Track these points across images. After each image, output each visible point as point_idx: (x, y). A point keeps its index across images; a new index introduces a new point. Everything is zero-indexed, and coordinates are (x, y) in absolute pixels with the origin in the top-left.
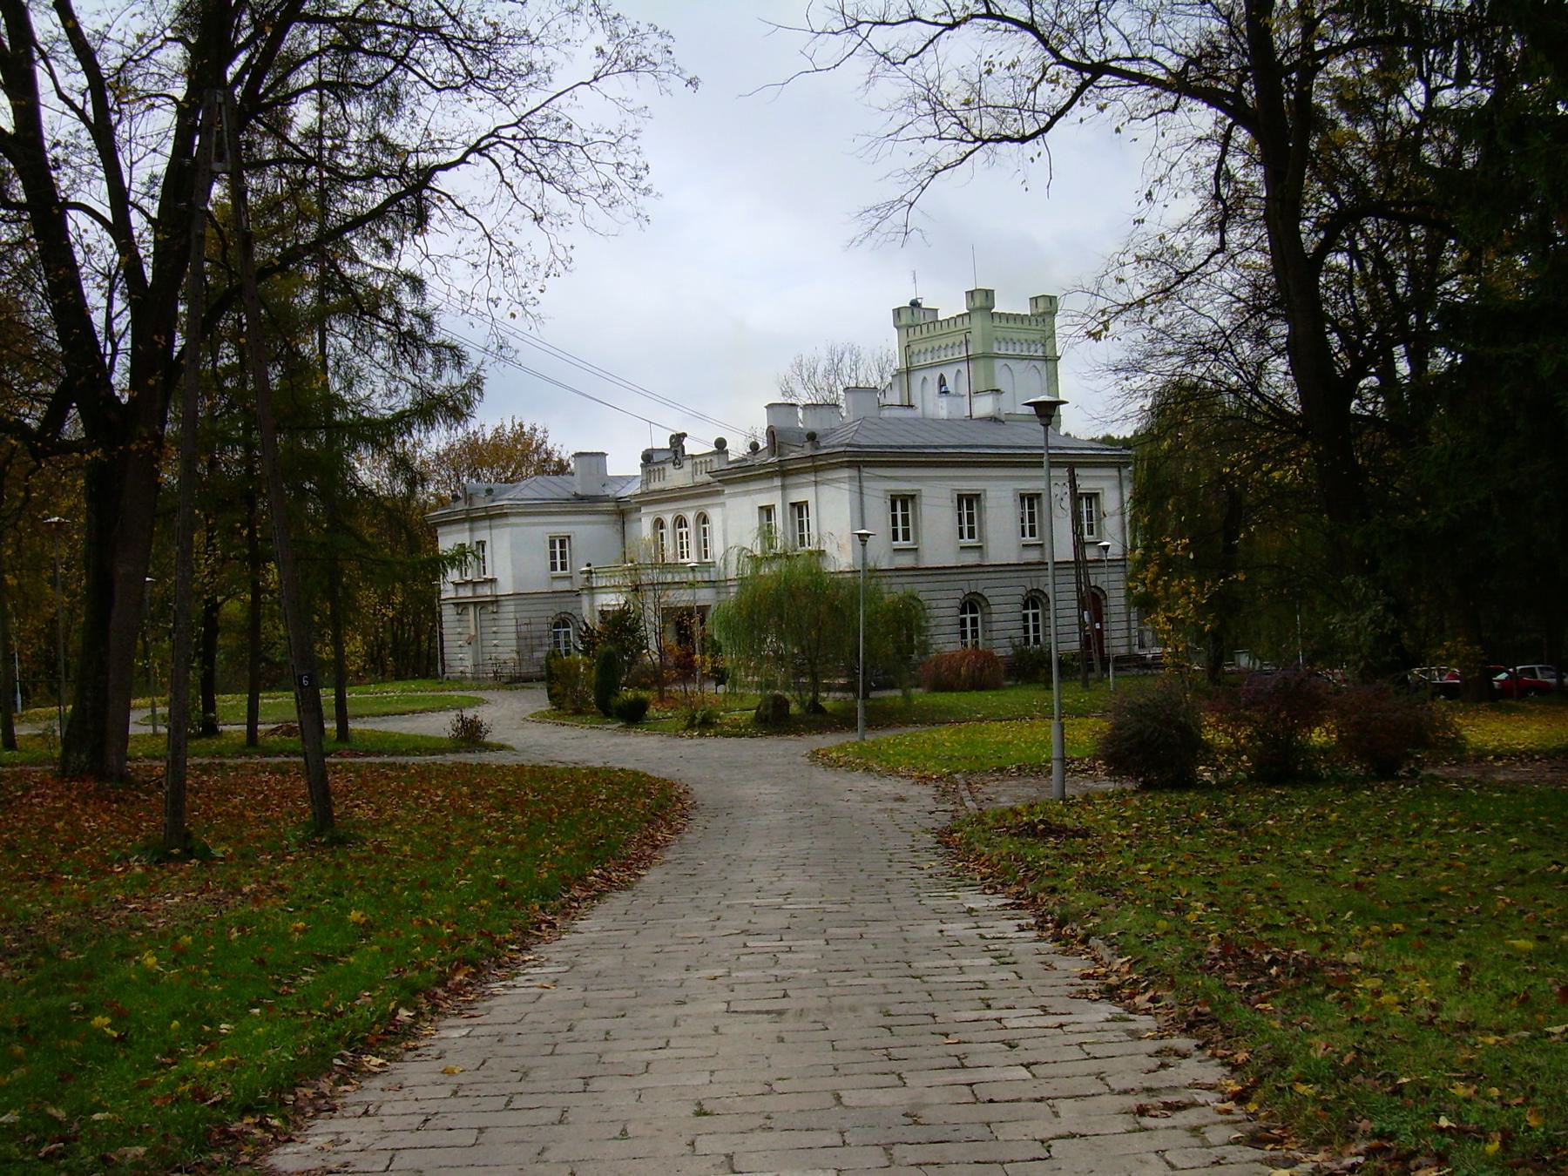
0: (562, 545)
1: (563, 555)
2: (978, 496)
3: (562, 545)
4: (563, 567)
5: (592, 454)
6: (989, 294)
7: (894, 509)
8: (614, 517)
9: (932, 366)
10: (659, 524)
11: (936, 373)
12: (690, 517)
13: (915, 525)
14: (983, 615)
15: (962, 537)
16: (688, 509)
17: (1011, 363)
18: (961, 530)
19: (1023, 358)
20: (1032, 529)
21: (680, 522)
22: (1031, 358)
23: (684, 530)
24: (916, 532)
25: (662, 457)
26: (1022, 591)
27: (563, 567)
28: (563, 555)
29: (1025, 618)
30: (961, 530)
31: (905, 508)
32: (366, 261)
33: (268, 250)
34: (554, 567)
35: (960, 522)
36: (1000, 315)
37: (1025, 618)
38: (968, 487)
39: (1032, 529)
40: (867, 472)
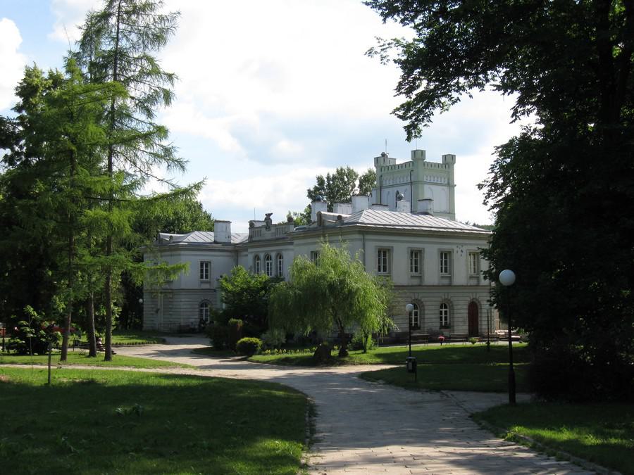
0: (207, 266)
1: (207, 271)
2: (420, 251)
3: (207, 266)
4: (207, 277)
5: (223, 222)
6: (423, 153)
7: (441, 257)
8: (233, 254)
9: (393, 186)
10: (257, 258)
11: (395, 189)
12: (273, 255)
13: (390, 264)
14: (421, 310)
15: (442, 272)
16: (272, 251)
17: (431, 186)
18: (412, 268)
19: (437, 184)
20: (268, 265)
21: (268, 257)
22: (441, 185)
23: (269, 262)
24: (390, 268)
25: (260, 225)
26: (440, 299)
27: (207, 277)
28: (207, 271)
29: (441, 313)
30: (379, 267)
31: (384, 255)
32: (139, 122)
33: (74, 117)
34: (202, 277)
35: (379, 263)
36: (428, 163)
37: (441, 313)
38: (446, 247)
39: (268, 265)
40: (368, 237)
